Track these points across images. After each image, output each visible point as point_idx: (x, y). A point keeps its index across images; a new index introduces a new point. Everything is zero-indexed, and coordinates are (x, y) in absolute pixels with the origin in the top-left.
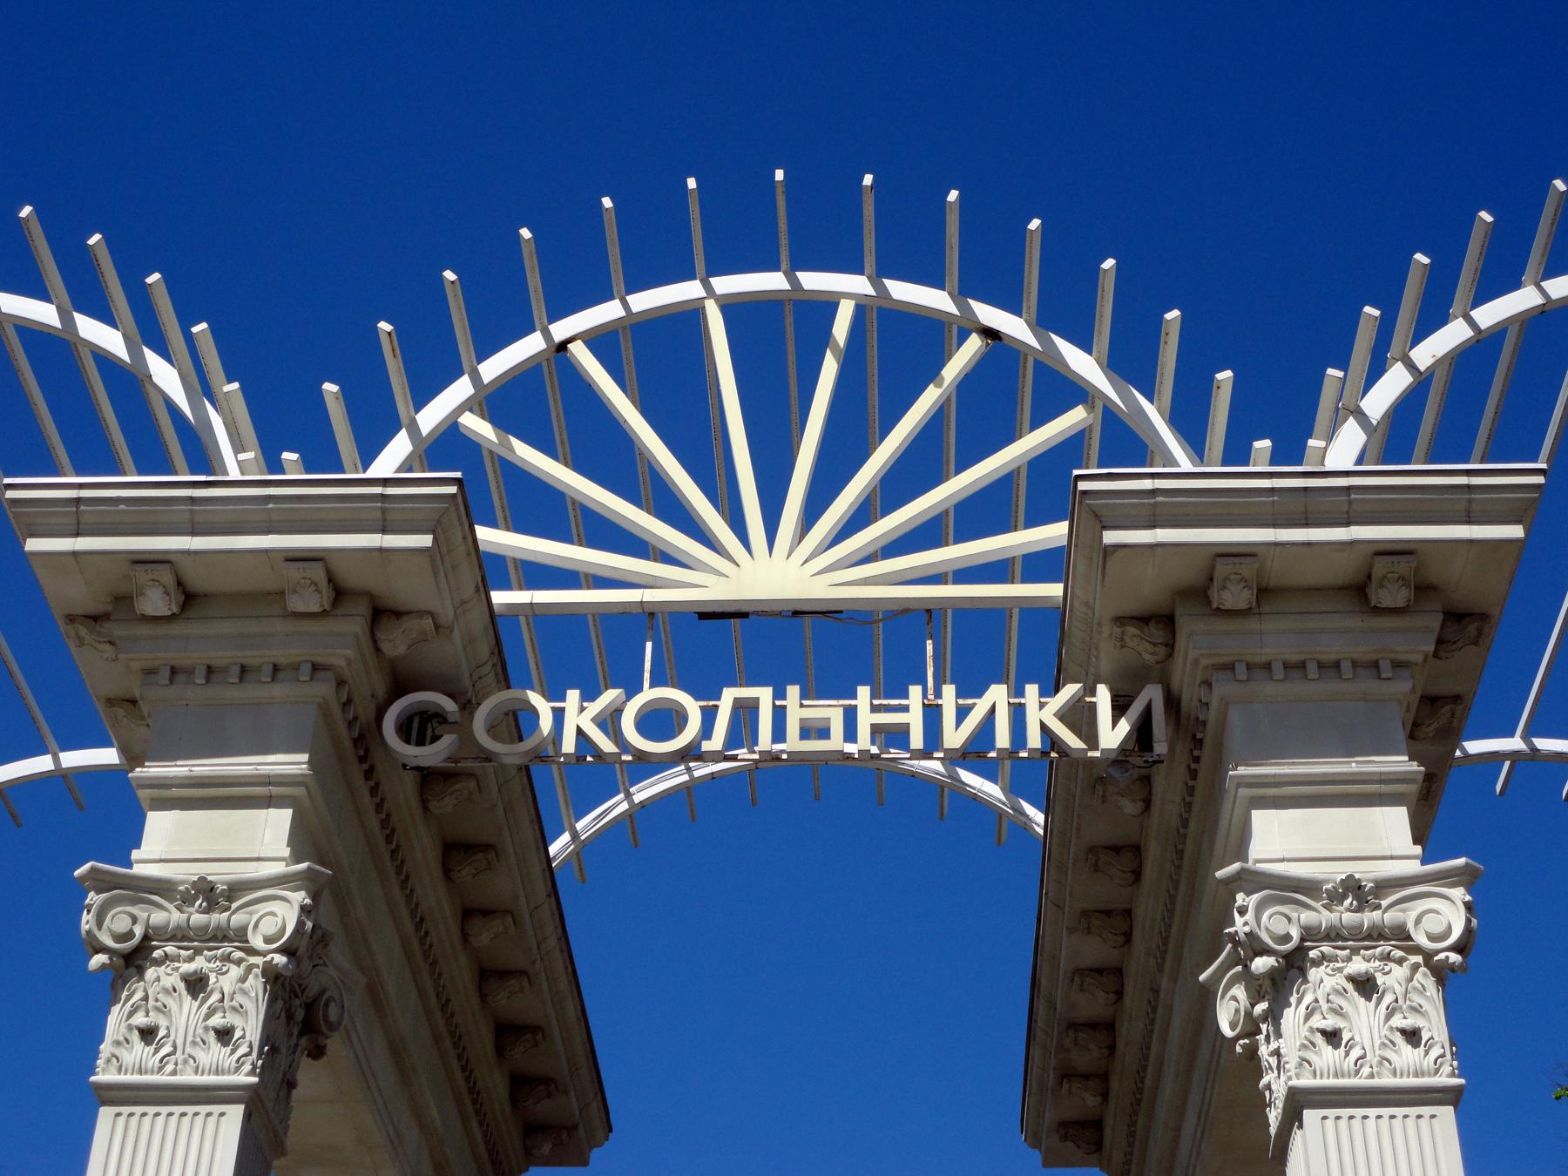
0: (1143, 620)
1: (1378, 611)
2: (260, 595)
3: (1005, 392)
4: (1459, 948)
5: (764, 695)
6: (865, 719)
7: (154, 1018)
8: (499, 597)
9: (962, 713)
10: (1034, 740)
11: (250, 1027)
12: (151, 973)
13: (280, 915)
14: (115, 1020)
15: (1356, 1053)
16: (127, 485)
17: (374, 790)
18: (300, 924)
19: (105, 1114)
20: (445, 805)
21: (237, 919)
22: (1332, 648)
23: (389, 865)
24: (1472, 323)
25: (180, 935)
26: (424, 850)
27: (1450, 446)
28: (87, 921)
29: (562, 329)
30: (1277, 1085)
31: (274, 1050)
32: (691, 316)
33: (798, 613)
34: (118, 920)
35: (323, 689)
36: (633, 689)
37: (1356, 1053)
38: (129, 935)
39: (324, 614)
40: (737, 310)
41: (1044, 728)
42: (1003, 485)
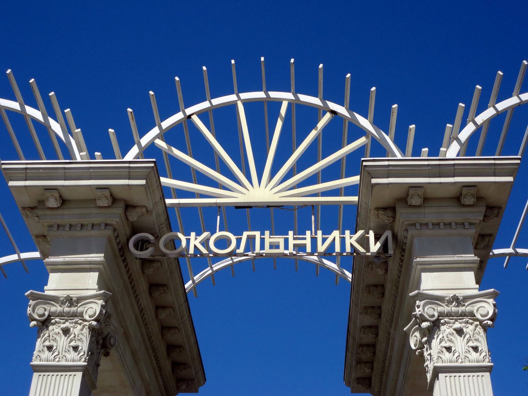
0: (385, 209)
2: (88, 200)
3: (338, 132)
4: (491, 319)
5: (257, 234)
6: (291, 242)
7: (52, 343)
8: (168, 201)
9: (324, 240)
10: (348, 249)
11: (84, 346)
12: (51, 328)
13: (94, 308)
14: (39, 344)
15: (457, 355)
16: (43, 163)
17: (126, 266)
18: (101, 311)
19: (36, 375)
20: (150, 271)
21: (80, 309)
22: (448, 218)
25: (61, 315)
26: (143, 286)
28: (29, 310)
29: (189, 111)
30: (430, 365)
31: (92, 354)
32: (233, 106)
33: (269, 206)
34: (40, 310)
35: (109, 232)
36: (213, 232)
37: (457, 355)
38: (44, 315)
39: (109, 207)
40: (248, 104)
41: (352, 245)
42: (338, 163)
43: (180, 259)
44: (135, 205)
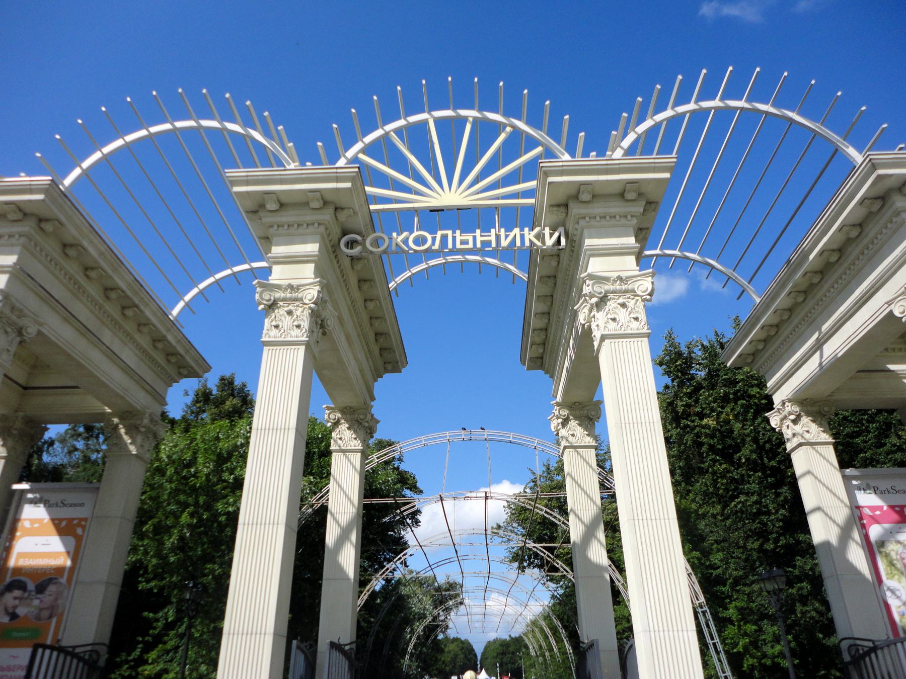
0: (559, 206)
1: (627, 201)
2: (302, 202)
3: (517, 144)
5: (450, 233)
7: (277, 323)
8: (372, 207)
9: (507, 236)
10: (527, 244)
11: (305, 324)
12: (276, 311)
13: (311, 294)
14: (267, 321)
16: (260, 172)
17: (338, 262)
19: (266, 349)
20: (359, 266)
21: (300, 295)
22: (613, 210)
24: (636, 133)
25: (284, 300)
26: (353, 281)
28: (257, 296)
30: (597, 334)
31: (312, 331)
32: (425, 123)
33: (459, 209)
34: (266, 296)
35: (322, 229)
36: (412, 232)
38: (270, 300)
39: (320, 209)
43: (384, 257)
44: (343, 206)
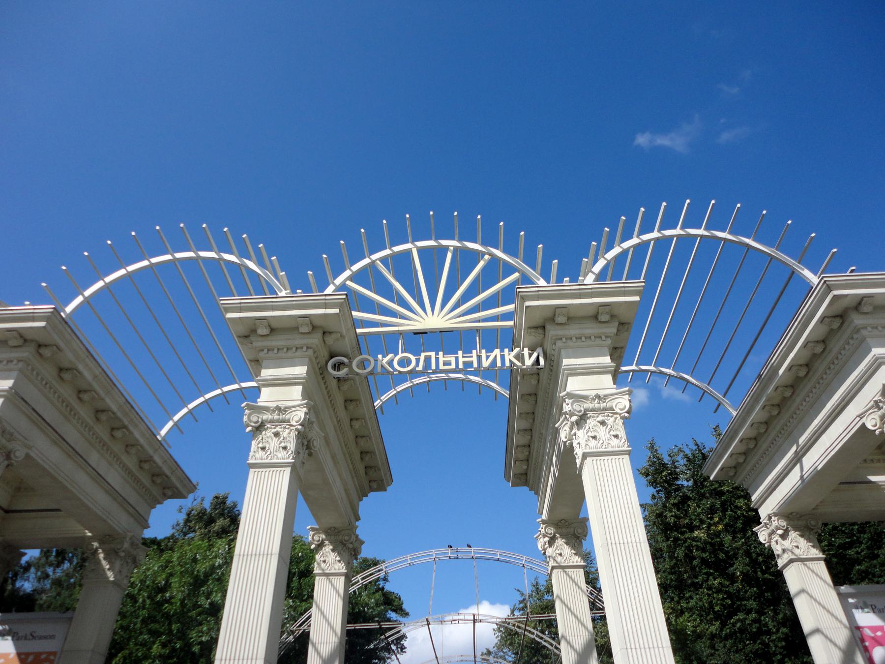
2: (290, 328)
4: (628, 412)
5: (433, 354)
6: (461, 360)
8: (359, 331)
9: (488, 357)
10: (508, 364)
12: (264, 433)
13: (299, 415)
15: (601, 442)
16: (254, 299)
17: (325, 383)
18: (305, 417)
19: (252, 471)
20: (345, 387)
22: (588, 332)
23: (330, 405)
27: (617, 276)
28: (245, 418)
29: (374, 257)
30: (579, 452)
31: (299, 453)
32: (408, 252)
34: (254, 418)
35: (310, 352)
36: (396, 354)
37: (601, 442)
38: (257, 422)
40: (421, 251)
41: (510, 361)
42: (495, 296)
